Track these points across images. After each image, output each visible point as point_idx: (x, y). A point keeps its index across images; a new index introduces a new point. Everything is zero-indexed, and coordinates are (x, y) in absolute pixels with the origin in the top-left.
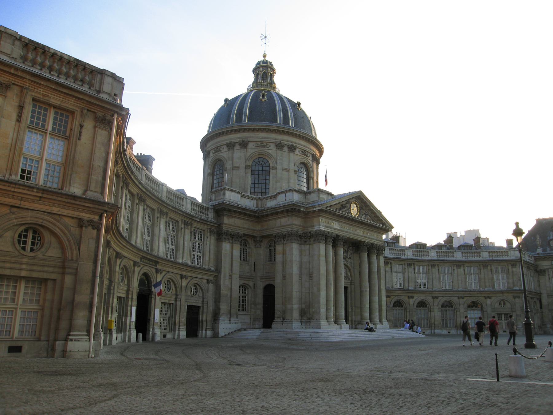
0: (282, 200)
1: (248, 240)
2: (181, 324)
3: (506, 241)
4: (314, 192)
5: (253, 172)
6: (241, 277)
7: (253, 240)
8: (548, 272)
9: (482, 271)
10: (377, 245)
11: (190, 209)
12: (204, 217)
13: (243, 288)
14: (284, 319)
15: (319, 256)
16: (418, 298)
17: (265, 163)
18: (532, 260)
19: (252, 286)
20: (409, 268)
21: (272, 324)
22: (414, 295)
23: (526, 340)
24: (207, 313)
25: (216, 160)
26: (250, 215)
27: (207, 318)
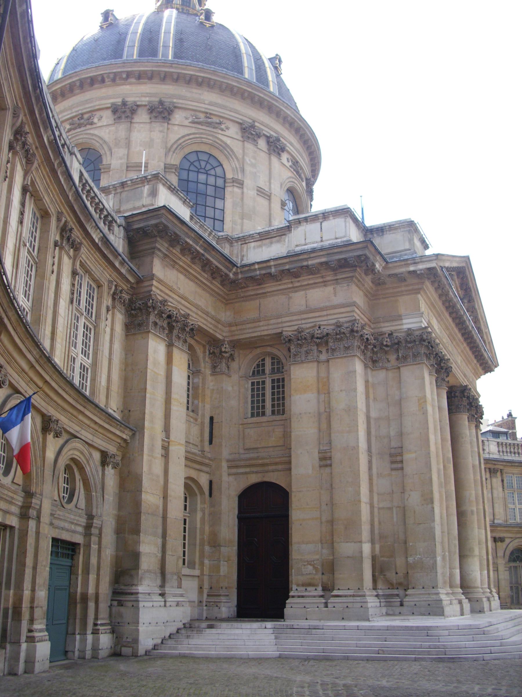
4: (396, 229)
14: (327, 589)
21: (284, 606)
23: (14, 427)
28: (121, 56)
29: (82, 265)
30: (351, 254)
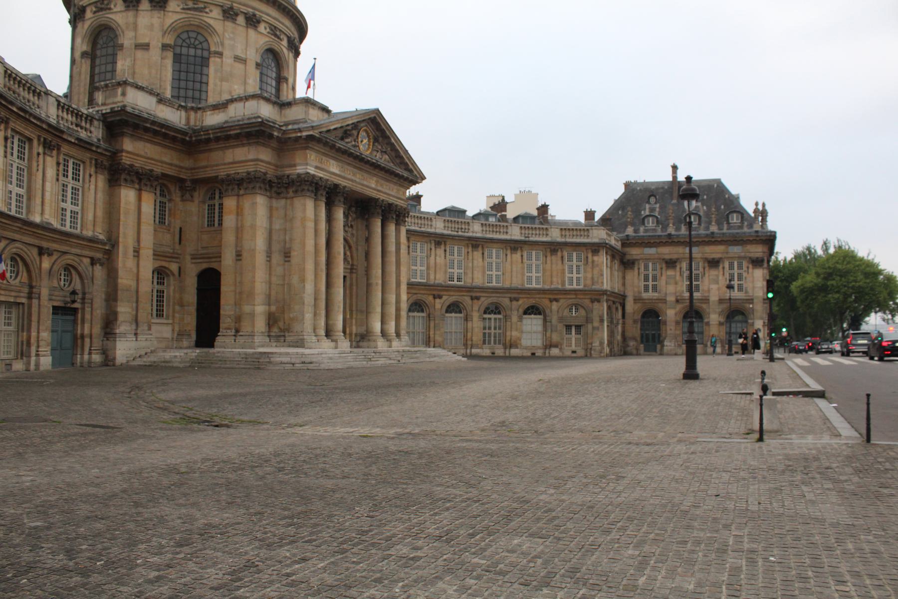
1: (172, 188)
2: (41, 343)
3: (584, 214)
6: (157, 255)
8: (639, 264)
10: (397, 206)
11: (55, 117)
12: (83, 135)
13: (160, 274)
14: (237, 331)
15: (304, 220)
16: (448, 299)
17: (201, 43)
18: (618, 245)
19: (176, 273)
22: (442, 293)
24: (91, 320)
25: (101, 25)
26: (174, 139)
27: (91, 331)
29: (13, 130)
30: (253, 129)
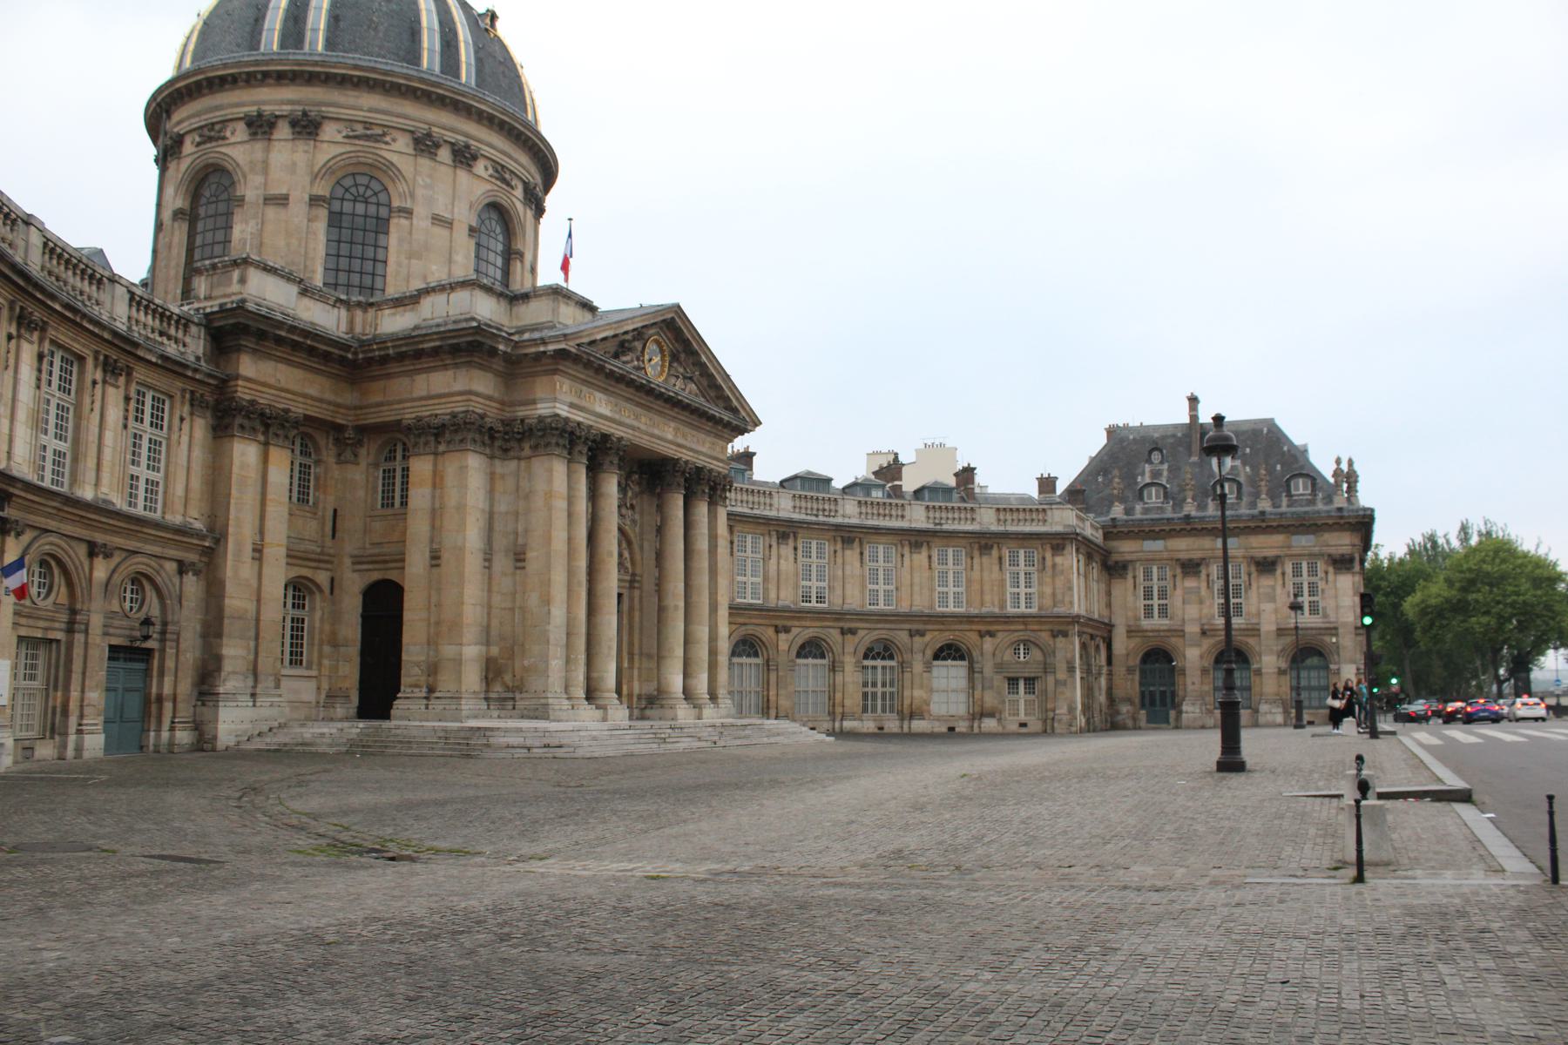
0: (435, 311)
2: (87, 711)
3: (1037, 483)
5: (335, 220)
6: (293, 557)
7: (331, 438)
8: (1134, 569)
9: (976, 560)
10: (711, 471)
11: (125, 320)
13: (299, 590)
14: (431, 690)
15: (549, 495)
16: (801, 633)
17: (376, 194)
18: (1098, 537)
19: (326, 586)
20: (783, 547)
21: (391, 707)
25: (207, 166)
26: (326, 357)
28: (257, 49)
